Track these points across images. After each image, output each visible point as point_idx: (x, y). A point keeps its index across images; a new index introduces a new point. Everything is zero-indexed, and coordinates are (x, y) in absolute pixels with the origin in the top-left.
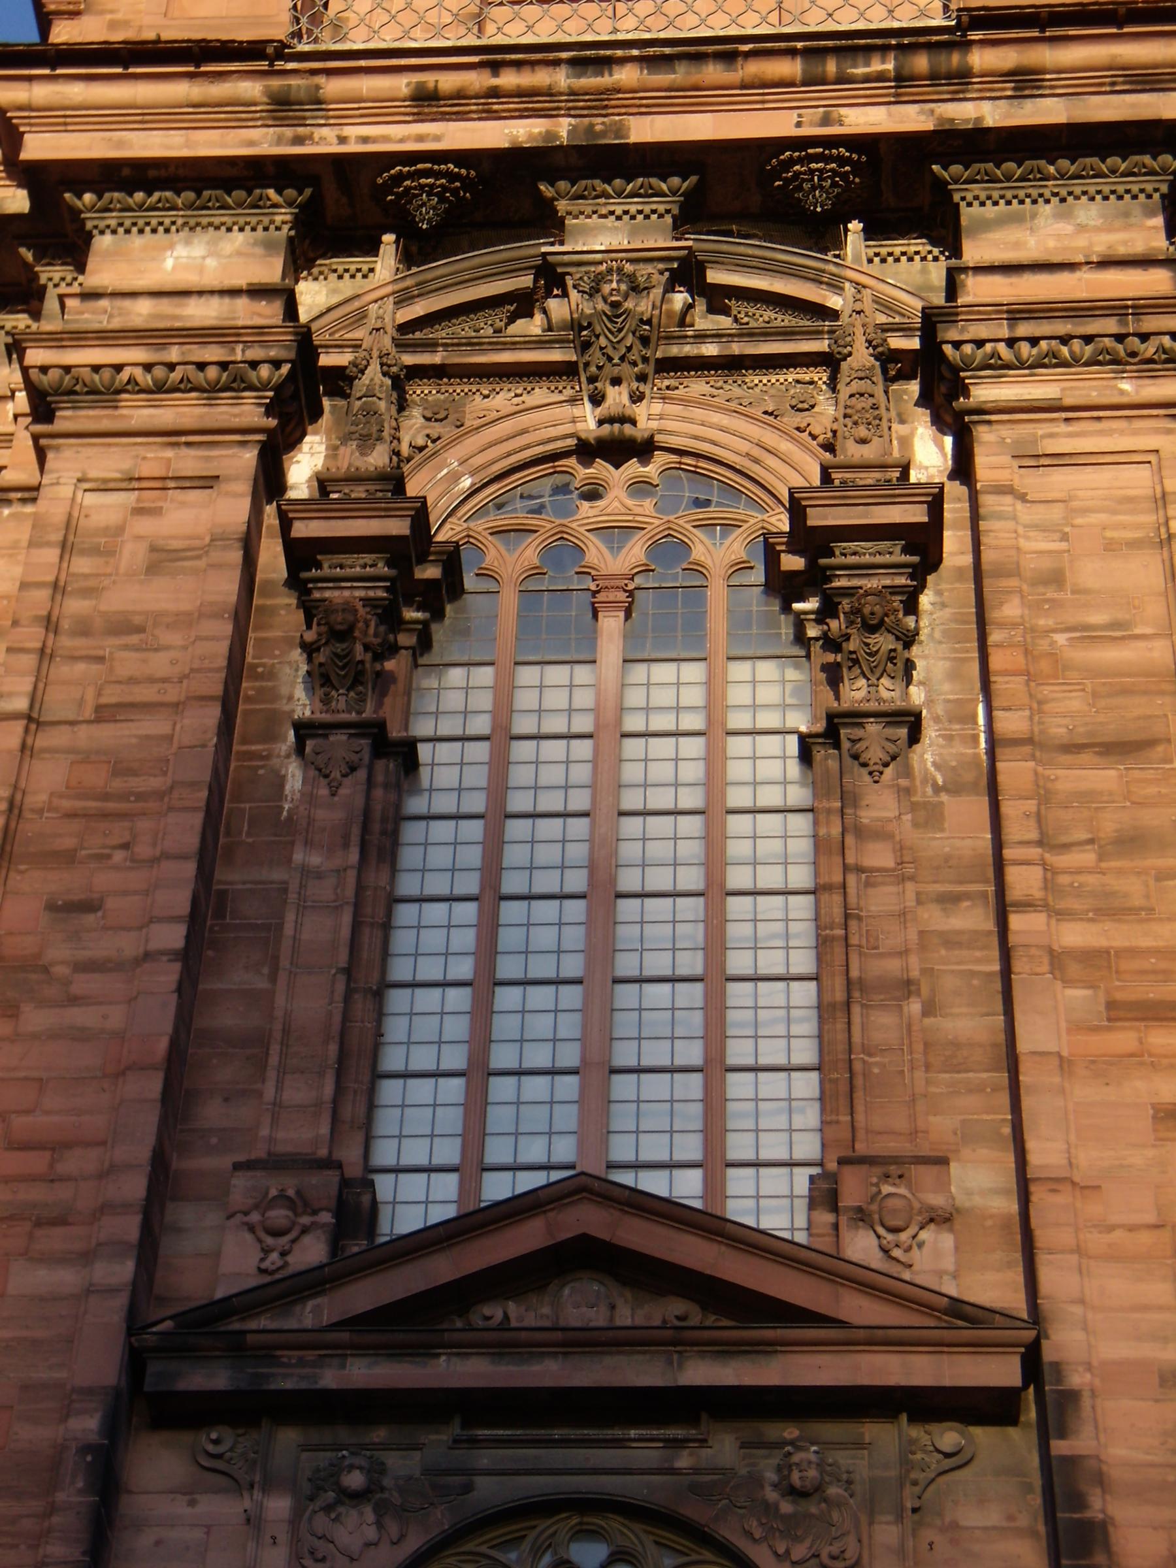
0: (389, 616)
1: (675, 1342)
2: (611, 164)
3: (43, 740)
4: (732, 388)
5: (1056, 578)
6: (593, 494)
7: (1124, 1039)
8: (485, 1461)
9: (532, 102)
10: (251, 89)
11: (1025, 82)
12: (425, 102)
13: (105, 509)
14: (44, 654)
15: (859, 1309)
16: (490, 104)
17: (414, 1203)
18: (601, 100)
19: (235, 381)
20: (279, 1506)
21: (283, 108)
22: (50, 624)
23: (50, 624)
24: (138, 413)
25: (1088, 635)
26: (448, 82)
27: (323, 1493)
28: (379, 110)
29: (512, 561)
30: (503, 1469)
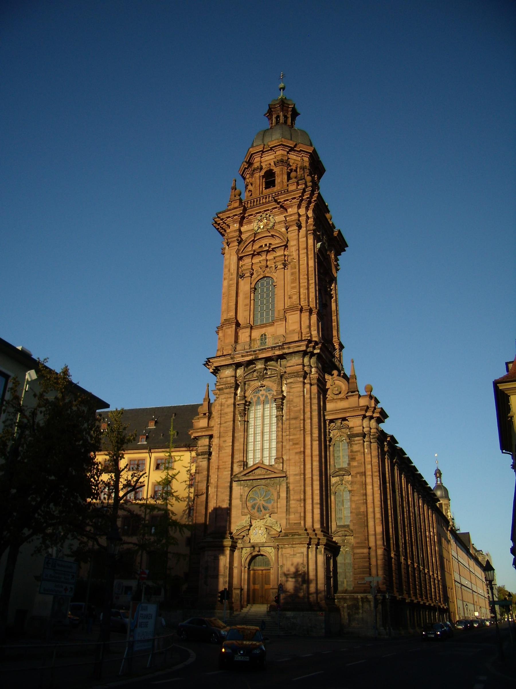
0: (245, 408)
1: (269, 474)
2: (257, 359)
3: (222, 425)
4: (270, 379)
5: (292, 401)
6: (261, 391)
7: (294, 447)
8: (439, 633)
9: (251, 355)
10: (229, 357)
11: (289, 348)
12: (242, 356)
13: (224, 401)
14: (221, 417)
15: (276, 471)
16: (248, 356)
17: (251, 463)
18: (256, 354)
19: (231, 387)
20: (242, 487)
21: (232, 358)
22: (221, 414)
23: (221, 414)
24: (225, 391)
25: (294, 407)
26: (244, 354)
27: (244, 486)
28: (239, 357)
29: (255, 399)
30: (255, 483)
